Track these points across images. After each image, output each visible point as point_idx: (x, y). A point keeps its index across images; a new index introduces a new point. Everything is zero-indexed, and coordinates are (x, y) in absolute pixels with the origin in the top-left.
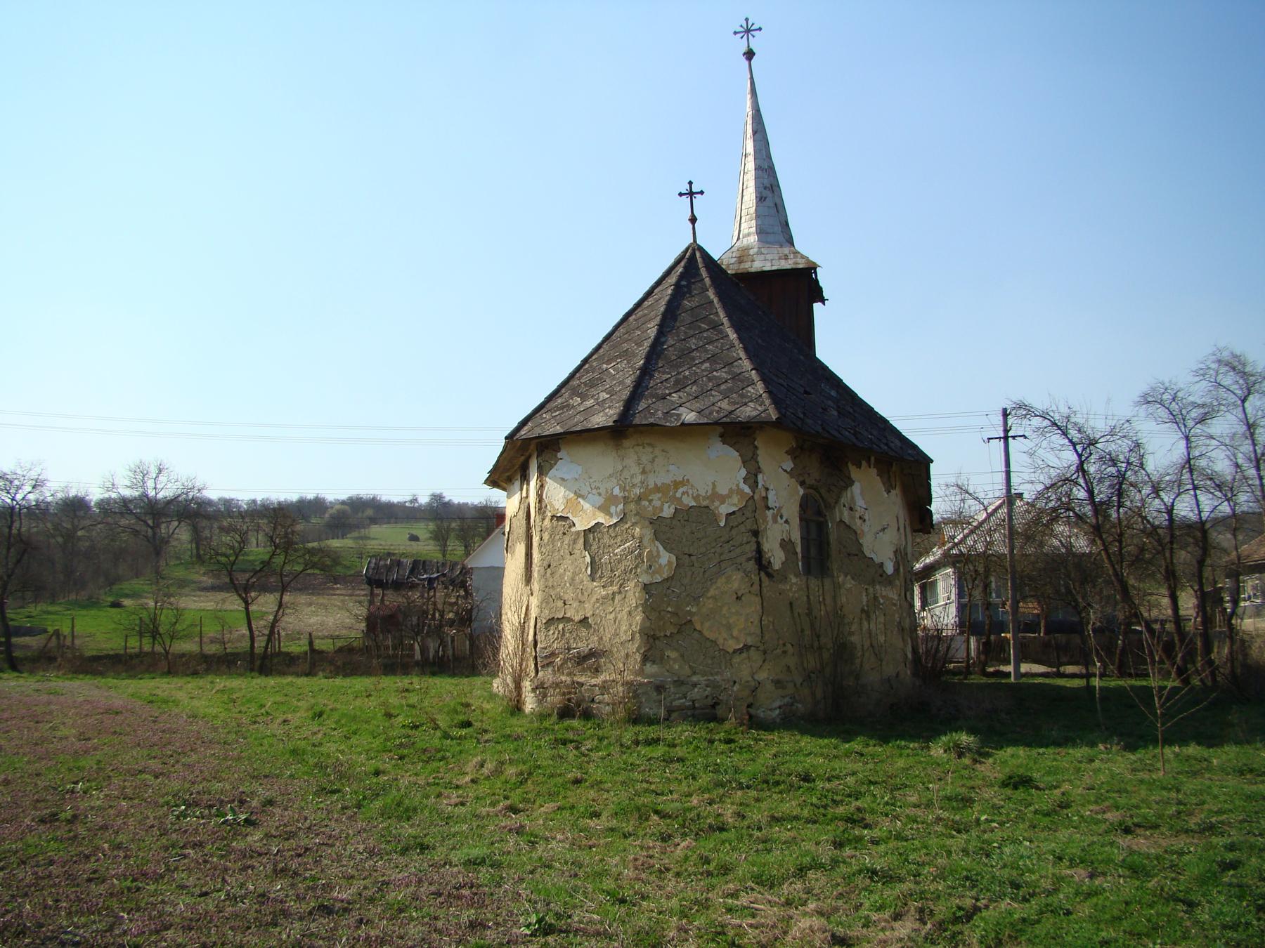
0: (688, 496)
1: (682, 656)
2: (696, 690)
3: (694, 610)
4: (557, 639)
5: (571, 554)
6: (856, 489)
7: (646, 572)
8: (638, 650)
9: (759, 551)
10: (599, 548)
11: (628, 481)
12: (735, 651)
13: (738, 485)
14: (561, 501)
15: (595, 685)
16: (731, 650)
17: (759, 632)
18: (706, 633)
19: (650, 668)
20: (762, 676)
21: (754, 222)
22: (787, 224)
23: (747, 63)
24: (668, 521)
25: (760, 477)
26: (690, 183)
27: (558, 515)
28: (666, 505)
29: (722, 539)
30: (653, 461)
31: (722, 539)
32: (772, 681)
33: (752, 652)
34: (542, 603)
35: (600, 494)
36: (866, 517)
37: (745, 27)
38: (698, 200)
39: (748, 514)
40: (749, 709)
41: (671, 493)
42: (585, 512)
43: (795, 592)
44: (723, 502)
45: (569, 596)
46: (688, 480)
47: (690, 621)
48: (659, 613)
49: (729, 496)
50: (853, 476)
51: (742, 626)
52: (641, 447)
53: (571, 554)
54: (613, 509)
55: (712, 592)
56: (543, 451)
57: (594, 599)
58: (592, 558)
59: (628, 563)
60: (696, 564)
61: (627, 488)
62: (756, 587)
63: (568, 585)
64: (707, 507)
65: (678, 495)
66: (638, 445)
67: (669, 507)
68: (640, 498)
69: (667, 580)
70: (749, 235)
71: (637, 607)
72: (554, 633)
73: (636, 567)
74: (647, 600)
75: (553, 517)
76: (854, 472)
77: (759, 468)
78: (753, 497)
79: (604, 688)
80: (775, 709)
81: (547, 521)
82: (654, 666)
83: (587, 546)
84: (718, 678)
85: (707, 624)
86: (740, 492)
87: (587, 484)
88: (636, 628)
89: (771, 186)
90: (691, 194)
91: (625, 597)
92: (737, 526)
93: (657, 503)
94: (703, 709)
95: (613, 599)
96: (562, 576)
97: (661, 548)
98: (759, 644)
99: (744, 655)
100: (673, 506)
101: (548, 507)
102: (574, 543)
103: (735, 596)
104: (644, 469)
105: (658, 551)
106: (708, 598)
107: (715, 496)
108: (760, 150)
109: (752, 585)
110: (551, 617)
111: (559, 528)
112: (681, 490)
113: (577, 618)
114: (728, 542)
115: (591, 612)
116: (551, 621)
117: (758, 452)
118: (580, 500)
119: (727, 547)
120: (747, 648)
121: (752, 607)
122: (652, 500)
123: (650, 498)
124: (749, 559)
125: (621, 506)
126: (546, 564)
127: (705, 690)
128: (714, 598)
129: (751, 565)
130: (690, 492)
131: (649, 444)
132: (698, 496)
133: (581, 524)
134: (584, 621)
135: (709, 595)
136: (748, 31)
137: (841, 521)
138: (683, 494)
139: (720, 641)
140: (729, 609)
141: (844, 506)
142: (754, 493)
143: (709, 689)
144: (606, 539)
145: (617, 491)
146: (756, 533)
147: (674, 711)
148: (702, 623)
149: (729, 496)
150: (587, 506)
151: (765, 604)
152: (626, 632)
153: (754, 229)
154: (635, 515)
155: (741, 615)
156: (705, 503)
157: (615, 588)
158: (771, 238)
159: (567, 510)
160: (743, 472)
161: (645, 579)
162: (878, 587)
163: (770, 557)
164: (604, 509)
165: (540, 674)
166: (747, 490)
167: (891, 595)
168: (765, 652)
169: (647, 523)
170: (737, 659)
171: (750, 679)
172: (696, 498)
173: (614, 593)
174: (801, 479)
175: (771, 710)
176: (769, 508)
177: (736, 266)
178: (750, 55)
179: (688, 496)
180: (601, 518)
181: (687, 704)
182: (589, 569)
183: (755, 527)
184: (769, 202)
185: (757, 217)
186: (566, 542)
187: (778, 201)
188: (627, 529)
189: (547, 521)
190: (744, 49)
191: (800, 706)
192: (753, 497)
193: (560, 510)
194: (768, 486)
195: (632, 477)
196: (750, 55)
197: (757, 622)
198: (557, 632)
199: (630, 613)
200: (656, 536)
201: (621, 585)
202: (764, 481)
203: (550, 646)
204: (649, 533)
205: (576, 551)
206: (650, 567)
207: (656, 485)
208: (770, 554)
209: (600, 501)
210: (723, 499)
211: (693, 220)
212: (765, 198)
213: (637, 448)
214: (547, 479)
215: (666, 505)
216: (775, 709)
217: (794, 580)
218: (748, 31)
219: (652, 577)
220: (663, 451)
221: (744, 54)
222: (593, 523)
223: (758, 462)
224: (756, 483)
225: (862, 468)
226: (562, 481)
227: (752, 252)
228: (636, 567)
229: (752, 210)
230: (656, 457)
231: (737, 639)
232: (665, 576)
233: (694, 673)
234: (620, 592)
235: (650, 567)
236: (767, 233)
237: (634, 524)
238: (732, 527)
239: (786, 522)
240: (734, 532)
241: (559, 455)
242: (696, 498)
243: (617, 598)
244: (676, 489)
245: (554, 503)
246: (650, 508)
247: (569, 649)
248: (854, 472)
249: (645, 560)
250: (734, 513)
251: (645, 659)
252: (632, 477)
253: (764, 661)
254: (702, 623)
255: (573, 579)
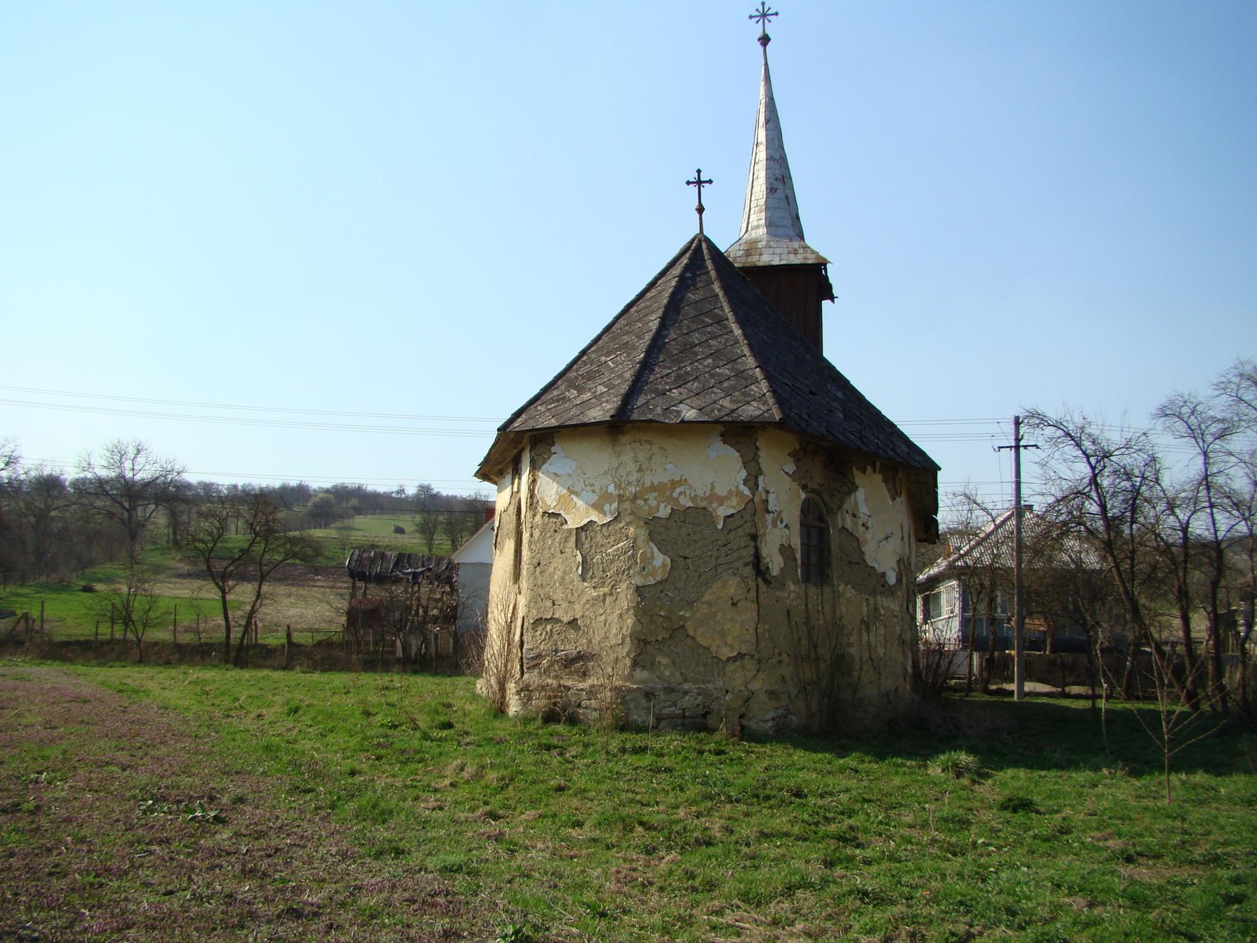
0: (686, 496)
1: (674, 662)
2: (687, 698)
3: (687, 615)
4: (544, 640)
5: (562, 553)
6: (860, 494)
7: (639, 574)
8: (628, 655)
9: (757, 556)
10: (591, 547)
11: (623, 478)
12: (729, 659)
13: (737, 487)
14: (553, 497)
15: (582, 690)
16: (724, 658)
17: (754, 639)
18: (699, 639)
19: (640, 674)
20: (756, 686)
21: (763, 214)
22: (798, 218)
23: (761, 49)
24: (664, 522)
25: (761, 479)
26: (699, 171)
27: (550, 512)
28: (662, 505)
29: (719, 542)
30: (650, 459)
31: (719, 542)
32: (766, 691)
33: (747, 661)
34: (530, 602)
35: (594, 491)
36: (869, 525)
37: (761, 10)
38: (706, 189)
39: (747, 517)
40: (741, 720)
41: (668, 493)
42: (578, 509)
43: (792, 600)
44: (721, 504)
45: (559, 595)
46: (686, 480)
47: (684, 626)
48: (651, 616)
49: (728, 498)
50: (857, 481)
51: (737, 634)
52: (638, 444)
53: (562, 553)
54: (607, 507)
55: (706, 597)
56: (536, 444)
57: (584, 600)
58: (584, 558)
59: (621, 564)
60: (691, 567)
61: (623, 486)
62: (753, 593)
63: (558, 584)
64: (705, 508)
65: (675, 495)
66: (635, 442)
67: (665, 507)
68: (635, 497)
69: (660, 582)
70: (758, 227)
71: (628, 610)
72: (541, 634)
73: (629, 569)
74: (638, 603)
75: (544, 513)
76: (858, 478)
77: (760, 469)
78: (752, 499)
79: (592, 692)
80: (768, 720)
81: (538, 517)
82: (645, 672)
83: (578, 544)
84: (710, 686)
85: (701, 630)
86: (739, 494)
87: (581, 480)
88: (625, 631)
89: (783, 177)
90: (699, 183)
91: (616, 599)
92: (735, 529)
93: (653, 503)
94: (693, 718)
95: (604, 601)
96: (552, 575)
97: (655, 549)
98: (753, 653)
99: (738, 663)
100: (670, 507)
101: (540, 503)
102: (566, 542)
103: (730, 602)
104: (640, 466)
105: (652, 553)
106: (703, 603)
107: (713, 497)
108: (773, 140)
109: (748, 591)
110: (538, 617)
111: (550, 525)
112: (678, 490)
113: (566, 620)
114: (725, 545)
115: (581, 614)
116: (538, 622)
117: (760, 453)
118: (573, 496)
119: (724, 550)
120: (741, 656)
121: (748, 613)
122: (648, 499)
123: (646, 497)
124: (746, 564)
125: (615, 505)
126: (535, 561)
127: (696, 699)
128: (709, 603)
129: (749, 571)
130: (688, 493)
131: (648, 442)
132: (696, 496)
133: (574, 522)
134: (573, 623)
135: (704, 600)
136: (764, 15)
137: (843, 527)
138: (680, 494)
139: (714, 648)
140: (724, 615)
141: (847, 512)
142: (754, 496)
143: (700, 697)
144: (599, 538)
145: (611, 489)
146: (754, 537)
147: (663, 719)
148: (695, 630)
149: (728, 498)
150: (580, 503)
151: (761, 611)
152: (616, 635)
153: (763, 222)
154: (630, 514)
155: (736, 621)
156: (703, 505)
157: (606, 590)
158: (780, 231)
159: (559, 507)
160: (744, 474)
161: (638, 581)
162: (879, 598)
163: (768, 563)
164: (597, 507)
165: (526, 676)
166: (747, 492)
167: (892, 606)
168: (759, 661)
169: (642, 523)
170: (730, 667)
171: (743, 688)
172: (693, 499)
173: (605, 595)
174: (803, 482)
175: (764, 721)
176: (768, 512)
177: (743, 260)
178: (765, 40)
179: (686, 496)
180: (594, 516)
181: (677, 712)
182: (580, 568)
183: (753, 531)
184: (780, 194)
185: (767, 208)
186: (557, 540)
187: (788, 192)
188: (621, 529)
189: (538, 517)
190: (759, 34)
191: (794, 718)
192: (752, 499)
193: (552, 506)
194: (769, 489)
195: (628, 475)
196: (765, 40)
197: (752, 630)
198: (544, 633)
199: (621, 616)
200: (651, 537)
201: (613, 587)
202: (765, 484)
203: (537, 647)
204: (643, 534)
205: (567, 550)
206: (644, 568)
207: (652, 484)
208: (768, 560)
209: (594, 498)
210: (721, 501)
211: (700, 210)
212: (776, 189)
213: (634, 445)
214: (540, 473)
215: (662, 505)
216: (768, 720)
217: (792, 587)
218: (764, 15)
219: (645, 579)
220: (661, 448)
221: (759, 39)
222: (585, 521)
223: (759, 464)
224: (757, 485)
225: (867, 473)
226: (555, 476)
227: (760, 245)
228: (629, 569)
229: (762, 202)
230: (653, 454)
231: (731, 647)
232: (659, 578)
233: (686, 680)
234: (611, 594)
235: (644, 568)
236: (777, 226)
237: (628, 524)
238: (730, 530)
239: (786, 526)
240: (732, 535)
241: (553, 449)
242: (693, 499)
243: (608, 599)
244: (673, 489)
245: (546, 499)
246: (646, 508)
247: (556, 651)
248: (858, 478)
249: (639, 561)
250: (732, 515)
251: (635, 664)
252: (628, 475)
253: (758, 671)
254: (695, 630)
255: (563, 579)
